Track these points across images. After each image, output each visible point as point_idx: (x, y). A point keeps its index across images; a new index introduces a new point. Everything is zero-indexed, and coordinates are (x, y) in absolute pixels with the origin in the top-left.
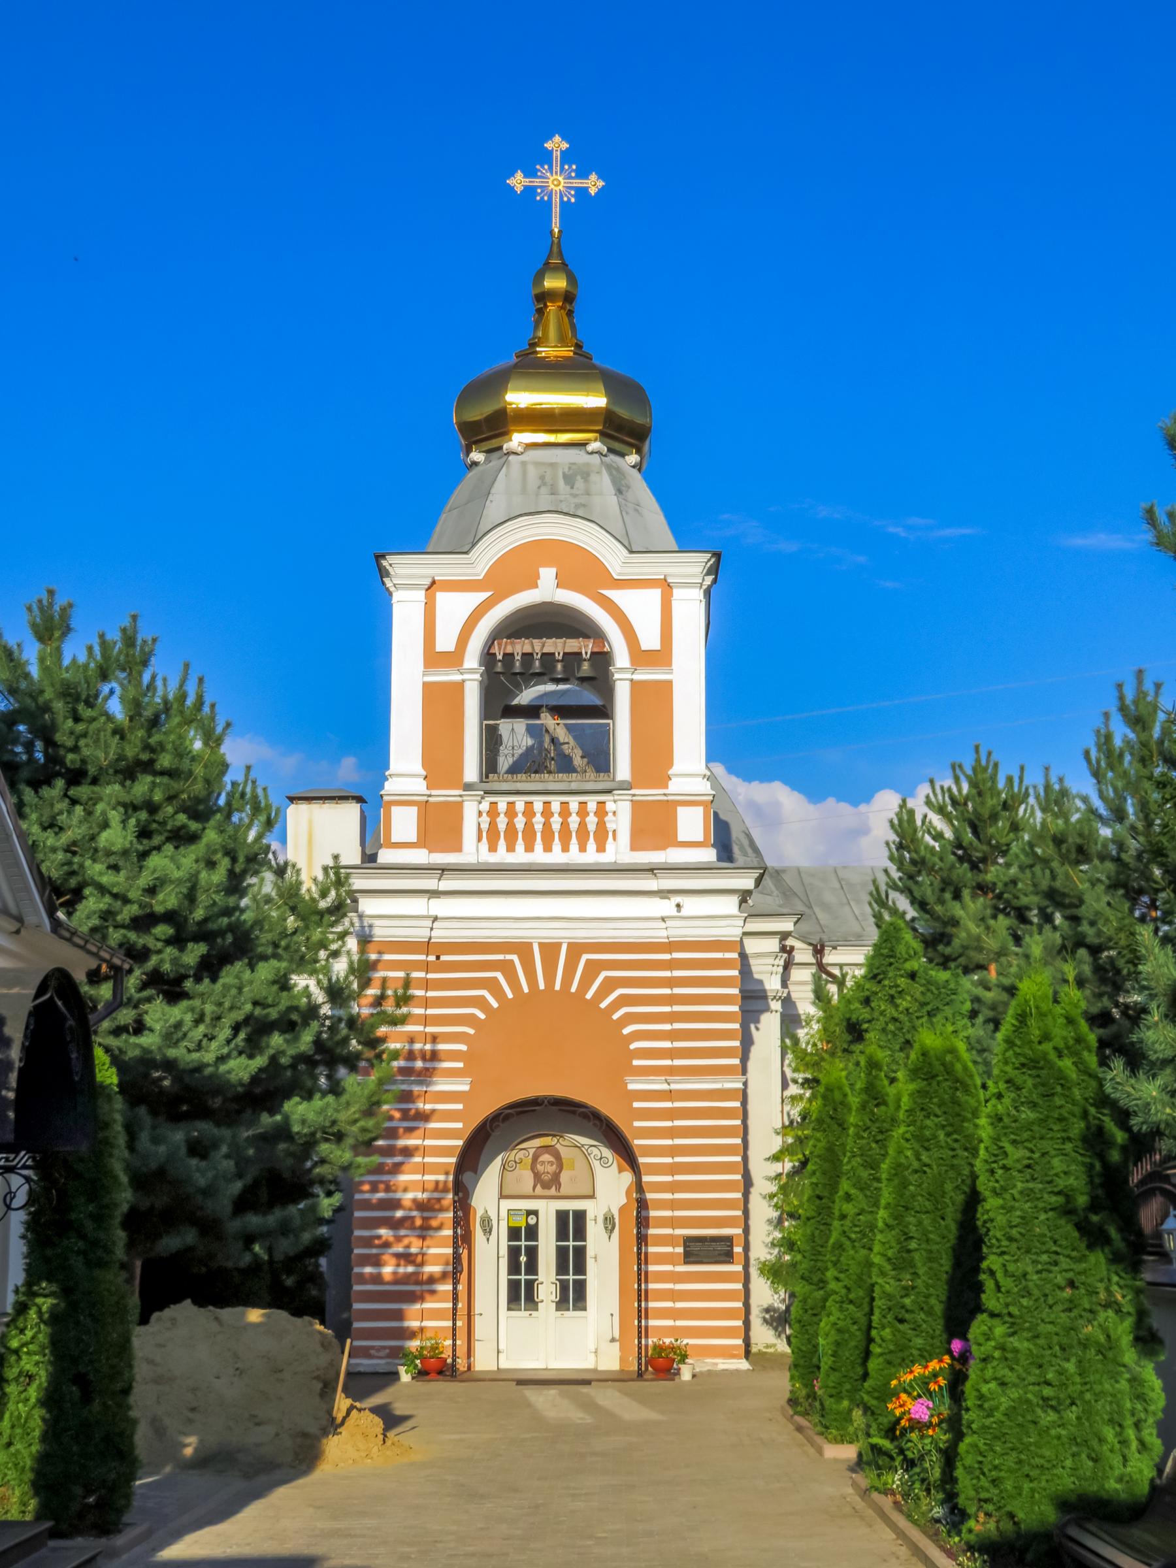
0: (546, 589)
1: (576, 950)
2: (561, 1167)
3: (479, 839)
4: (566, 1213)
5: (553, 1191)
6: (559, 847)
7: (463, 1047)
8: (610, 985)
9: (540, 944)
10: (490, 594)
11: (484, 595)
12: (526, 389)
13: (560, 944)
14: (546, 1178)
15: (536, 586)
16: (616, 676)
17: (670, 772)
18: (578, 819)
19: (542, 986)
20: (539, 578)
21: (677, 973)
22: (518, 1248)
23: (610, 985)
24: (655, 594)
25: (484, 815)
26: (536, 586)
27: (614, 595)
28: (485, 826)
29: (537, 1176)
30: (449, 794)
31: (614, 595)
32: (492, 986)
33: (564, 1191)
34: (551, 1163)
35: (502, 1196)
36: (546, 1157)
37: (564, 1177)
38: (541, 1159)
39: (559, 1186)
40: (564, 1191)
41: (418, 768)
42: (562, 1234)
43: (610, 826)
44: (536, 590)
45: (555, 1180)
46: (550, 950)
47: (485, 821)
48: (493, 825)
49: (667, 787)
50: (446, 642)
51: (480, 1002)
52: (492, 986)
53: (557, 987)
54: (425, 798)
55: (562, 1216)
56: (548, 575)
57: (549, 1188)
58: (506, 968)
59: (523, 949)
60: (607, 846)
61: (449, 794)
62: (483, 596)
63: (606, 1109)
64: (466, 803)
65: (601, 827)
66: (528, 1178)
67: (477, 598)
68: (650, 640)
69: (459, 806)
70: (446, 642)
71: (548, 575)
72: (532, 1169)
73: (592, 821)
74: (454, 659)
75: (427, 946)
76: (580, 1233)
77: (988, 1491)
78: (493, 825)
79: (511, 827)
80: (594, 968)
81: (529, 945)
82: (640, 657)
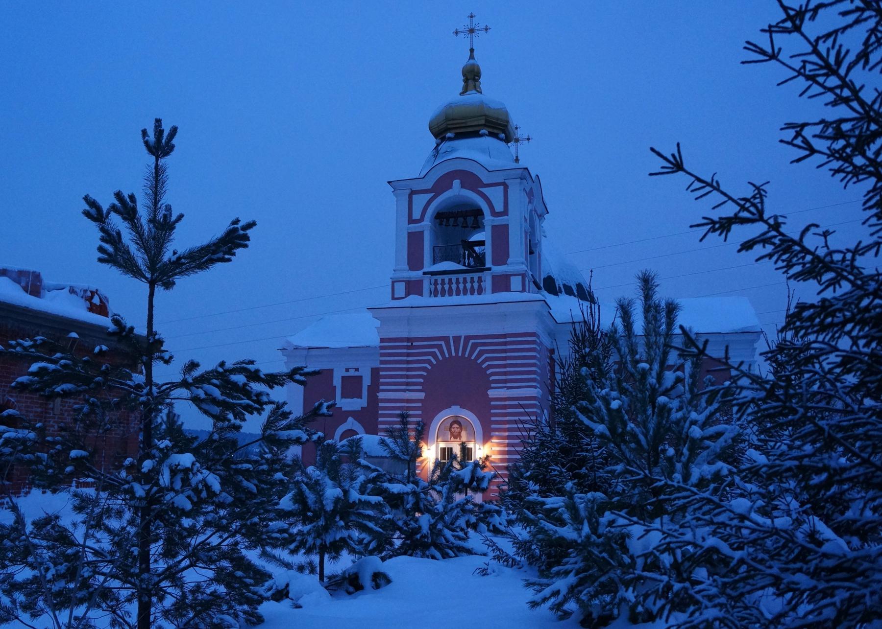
0: (456, 191)
1: (468, 338)
7: (420, 405)
8: (481, 353)
11: (432, 194)
12: (450, 198)
19: (454, 354)
21: (508, 369)
23: (481, 353)
24: (502, 187)
27: (484, 190)
28: (433, 289)
31: (484, 190)
32: (434, 355)
36: (456, 426)
46: (457, 339)
47: (433, 287)
48: (436, 289)
50: (416, 215)
51: (429, 362)
52: (434, 355)
58: (439, 347)
59: (446, 339)
63: (491, 199)
67: (429, 196)
68: (499, 208)
70: (416, 215)
71: (457, 183)
73: (476, 285)
75: (408, 340)
77: (802, 337)
78: (436, 289)
80: (475, 346)
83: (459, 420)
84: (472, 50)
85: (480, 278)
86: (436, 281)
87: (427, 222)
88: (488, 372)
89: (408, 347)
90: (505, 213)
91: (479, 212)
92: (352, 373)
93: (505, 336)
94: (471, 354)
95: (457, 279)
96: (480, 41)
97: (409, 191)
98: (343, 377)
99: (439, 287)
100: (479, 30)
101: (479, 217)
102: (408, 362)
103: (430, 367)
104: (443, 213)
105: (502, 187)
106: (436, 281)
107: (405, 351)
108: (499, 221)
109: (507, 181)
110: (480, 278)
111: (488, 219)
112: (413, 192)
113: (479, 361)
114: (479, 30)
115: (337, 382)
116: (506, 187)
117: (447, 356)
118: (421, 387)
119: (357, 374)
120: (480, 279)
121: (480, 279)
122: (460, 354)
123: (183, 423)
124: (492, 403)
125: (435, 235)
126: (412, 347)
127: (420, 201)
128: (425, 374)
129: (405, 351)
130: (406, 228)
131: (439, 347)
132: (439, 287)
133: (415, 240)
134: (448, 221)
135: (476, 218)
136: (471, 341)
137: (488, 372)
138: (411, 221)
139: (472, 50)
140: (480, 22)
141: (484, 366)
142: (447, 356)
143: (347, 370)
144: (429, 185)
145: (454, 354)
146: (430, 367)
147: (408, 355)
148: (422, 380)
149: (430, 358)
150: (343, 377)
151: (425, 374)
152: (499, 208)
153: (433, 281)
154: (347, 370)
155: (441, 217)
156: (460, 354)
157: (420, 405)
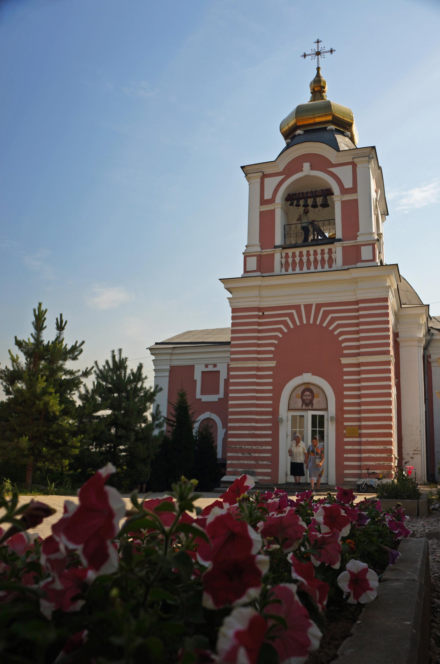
1: (319, 306)
2: (313, 397)
3: (282, 267)
4: (316, 415)
5: (310, 407)
6: (321, 267)
7: (271, 373)
9: (305, 306)
10: (284, 176)
13: (312, 304)
14: (307, 401)
15: (302, 171)
16: (335, 199)
17: (358, 233)
18: (328, 255)
20: (303, 167)
22: (300, 428)
24: (351, 166)
25: (283, 258)
26: (302, 171)
27: (332, 170)
28: (284, 262)
29: (303, 401)
30: (269, 251)
31: (332, 170)
32: (285, 323)
33: (315, 407)
34: (309, 395)
35: (289, 409)
36: (307, 393)
37: (315, 401)
38: (305, 394)
39: (312, 405)
40: (315, 407)
41: (258, 243)
42: (314, 425)
43: (333, 257)
44: (302, 172)
45: (311, 403)
46: (308, 307)
47: (284, 261)
48: (287, 262)
49: (357, 239)
50: (268, 196)
51: (280, 330)
52: (285, 323)
53: (292, 327)
54: (259, 253)
55: (314, 417)
56: (306, 166)
57: (308, 406)
58: (291, 316)
59: (297, 308)
60: (333, 266)
61: (269, 251)
62: (281, 177)
64: (275, 254)
65: (330, 258)
66: (300, 401)
68: (348, 184)
69: (273, 255)
70: (268, 196)
71: (306, 166)
72: (301, 398)
73: (326, 257)
74: (272, 201)
76: (322, 425)
78: (287, 262)
79: (301, 261)
80: (326, 314)
81: (300, 306)
82: (344, 191)
83: (311, 387)
84: (318, 69)
85: (330, 250)
86: (287, 254)
87: (279, 198)
88: (341, 339)
89: (259, 317)
90: (354, 190)
91: (329, 192)
92: (211, 368)
93: (357, 303)
94: (323, 320)
95: (308, 252)
96: (325, 61)
97: (261, 174)
98: (203, 372)
99: (290, 260)
100: (325, 52)
101: (328, 197)
102: (259, 338)
103: (281, 336)
104: (294, 194)
105: (351, 166)
106: (287, 254)
107: (256, 320)
108: (347, 197)
109: (355, 160)
110: (330, 250)
111: (337, 200)
112: (264, 176)
113: (331, 328)
114: (325, 52)
115: (198, 376)
116: (354, 165)
117: (298, 324)
118: (271, 356)
119: (215, 369)
120: (330, 250)
121: (330, 250)
122: (311, 322)
123: (63, 339)
124: (345, 369)
125: (286, 213)
126: (263, 316)
127: (271, 184)
128: (276, 342)
129: (256, 320)
130: (258, 208)
131: (291, 316)
132: (290, 260)
133: (265, 222)
134: (298, 201)
135: (325, 197)
136: (323, 309)
137: (341, 339)
138: (263, 202)
139: (318, 69)
140: (325, 46)
141: (336, 333)
142: (298, 324)
143: (206, 366)
144: (281, 168)
145: (305, 322)
146: (281, 336)
147: (259, 324)
148: (273, 349)
149: (282, 326)
150: (203, 372)
151: (276, 342)
152: (348, 184)
153: (284, 255)
154: (206, 366)
155: (291, 198)
156: (311, 322)
157: (271, 373)
